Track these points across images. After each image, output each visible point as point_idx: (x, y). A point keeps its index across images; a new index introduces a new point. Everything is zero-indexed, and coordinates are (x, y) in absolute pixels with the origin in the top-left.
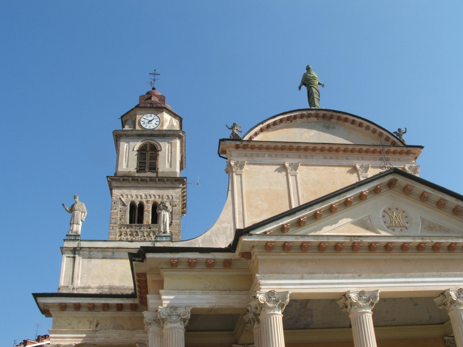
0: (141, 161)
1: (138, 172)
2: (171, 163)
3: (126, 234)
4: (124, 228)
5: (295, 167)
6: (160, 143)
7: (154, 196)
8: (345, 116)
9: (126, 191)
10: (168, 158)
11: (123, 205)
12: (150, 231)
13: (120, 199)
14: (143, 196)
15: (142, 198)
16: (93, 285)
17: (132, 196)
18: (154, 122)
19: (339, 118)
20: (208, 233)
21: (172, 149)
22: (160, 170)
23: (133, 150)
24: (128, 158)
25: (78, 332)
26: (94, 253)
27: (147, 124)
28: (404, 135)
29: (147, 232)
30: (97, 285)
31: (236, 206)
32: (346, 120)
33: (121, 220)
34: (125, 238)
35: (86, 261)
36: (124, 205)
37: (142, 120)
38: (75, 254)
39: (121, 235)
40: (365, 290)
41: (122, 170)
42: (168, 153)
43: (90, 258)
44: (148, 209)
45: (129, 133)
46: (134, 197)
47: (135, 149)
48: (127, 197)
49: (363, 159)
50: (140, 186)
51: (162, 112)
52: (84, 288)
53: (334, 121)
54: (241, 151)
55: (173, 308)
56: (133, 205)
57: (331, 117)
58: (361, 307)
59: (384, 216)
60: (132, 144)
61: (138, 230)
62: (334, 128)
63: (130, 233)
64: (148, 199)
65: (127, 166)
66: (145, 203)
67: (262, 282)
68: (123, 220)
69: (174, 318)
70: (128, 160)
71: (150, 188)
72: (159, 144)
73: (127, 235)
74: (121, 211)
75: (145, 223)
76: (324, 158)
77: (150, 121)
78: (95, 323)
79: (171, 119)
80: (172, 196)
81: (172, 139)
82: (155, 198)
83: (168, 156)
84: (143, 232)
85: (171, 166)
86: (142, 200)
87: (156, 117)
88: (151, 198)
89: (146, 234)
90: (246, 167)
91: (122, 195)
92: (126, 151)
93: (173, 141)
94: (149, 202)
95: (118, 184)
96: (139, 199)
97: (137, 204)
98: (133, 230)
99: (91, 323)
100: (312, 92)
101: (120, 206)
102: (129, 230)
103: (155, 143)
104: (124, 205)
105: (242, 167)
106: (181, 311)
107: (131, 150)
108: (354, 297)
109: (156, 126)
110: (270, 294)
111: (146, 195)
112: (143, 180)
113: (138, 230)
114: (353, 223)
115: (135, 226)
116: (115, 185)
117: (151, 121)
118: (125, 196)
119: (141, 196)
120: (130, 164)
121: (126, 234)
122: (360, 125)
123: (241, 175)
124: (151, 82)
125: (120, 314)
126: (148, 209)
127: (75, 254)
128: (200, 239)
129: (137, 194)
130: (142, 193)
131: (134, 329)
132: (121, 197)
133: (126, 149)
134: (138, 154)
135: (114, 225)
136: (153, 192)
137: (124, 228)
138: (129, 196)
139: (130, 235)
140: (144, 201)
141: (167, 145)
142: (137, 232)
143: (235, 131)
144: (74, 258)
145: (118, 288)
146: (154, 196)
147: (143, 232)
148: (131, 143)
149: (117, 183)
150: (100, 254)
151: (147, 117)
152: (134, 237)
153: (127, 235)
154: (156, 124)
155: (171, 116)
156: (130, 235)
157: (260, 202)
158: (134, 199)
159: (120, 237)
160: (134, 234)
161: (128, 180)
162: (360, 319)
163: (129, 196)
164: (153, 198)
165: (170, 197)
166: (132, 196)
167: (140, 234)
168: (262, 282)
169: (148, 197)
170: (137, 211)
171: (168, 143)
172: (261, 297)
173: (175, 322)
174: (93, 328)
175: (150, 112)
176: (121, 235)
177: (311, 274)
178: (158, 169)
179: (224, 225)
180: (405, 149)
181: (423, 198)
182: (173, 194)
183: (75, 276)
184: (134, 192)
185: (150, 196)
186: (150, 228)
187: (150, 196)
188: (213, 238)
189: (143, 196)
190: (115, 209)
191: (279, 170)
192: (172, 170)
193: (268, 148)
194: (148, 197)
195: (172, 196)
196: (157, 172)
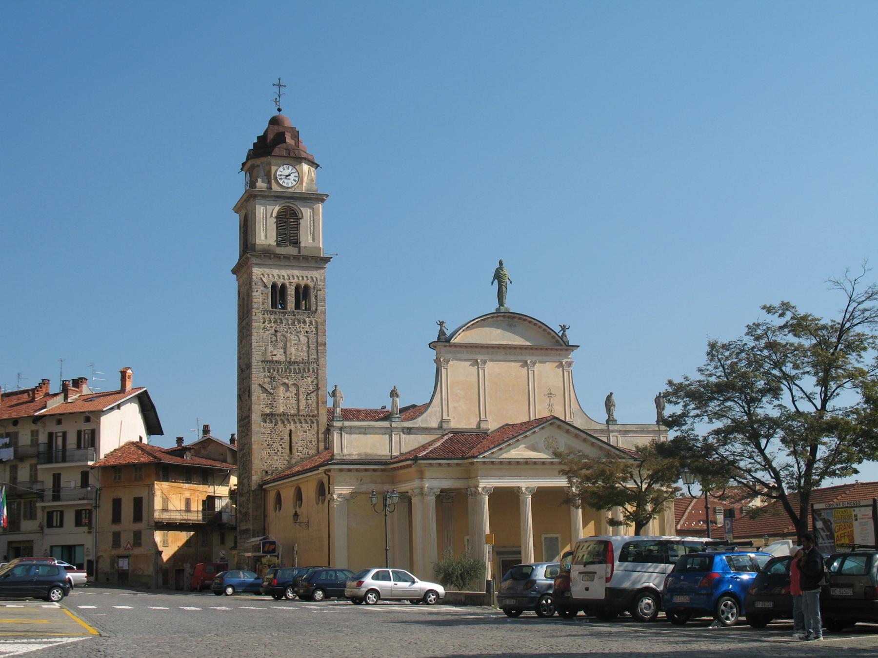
0: (281, 231)
1: (278, 245)
2: (314, 235)
3: (270, 321)
4: (268, 314)
5: (484, 362)
6: (301, 209)
7: (297, 276)
8: (525, 318)
9: (267, 271)
10: (310, 229)
11: (265, 287)
12: (294, 319)
13: (261, 278)
14: (286, 277)
15: (284, 279)
16: (355, 453)
17: (273, 276)
18: (292, 177)
19: (520, 319)
20: (425, 415)
21: (315, 217)
22: (302, 245)
23: (271, 216)
24: (266, 226)
25: (351, 486)
26: (353, 430)
27: (285, 180)
28: (567, 330)
29: (291, 319)
30: (357, 453)
31: (443, 395)
32: (525, 320)
33: (263, 304)
34: (269, 326)
35: (348, 435)
36: (265, 286)
37: (278, 173)
38: (341, 431)
39: (264, 323)
40: (530, 486)
41: (260, 242)
42: (310, 222)
43: (351, 433)
44: (291, 292)
45: (267, 194)
46: (276, 277)
47: (274, 215)
48: (269, 277)
49: (533, 354)
50: (282, 264)
51: (301, 163)
52: (349, 455)
53: (516, 320)
54: (448, 348)
55: (431, 489)
56: (274, 286)
57: (514, 317)
58: (526, 495)
59: (544, 442)
60: (270, 208)
61: (282, 318)
62: (515, 326)
63: (274, 320)
64: (291, 281)
65: (266, 237)
66: (288, 285)
67: (480, 481)
68: (265, 305)
69: (432, 494)
70: (266, 228)
71: (293, 267)
72: (300, 209)
73: (271, 322)
74: (262, 294)
75: (289, 309)
76: (506, 354)
77: (287, 176)
78: (360, 479)
79: (309, 168)
80: (316, 277)
81: (314, 204)
82: (299, 279)
83: (310, 225)
84: (287, 320)
85: (313, 240)
86: (285, 281)
87: (294, 170)
88: (294, 279)
89: (290, 322)
90: (451, 363)
91: (262, 274)
92: (263, 217)
93: (315, 207)
94: (293, 284)
95: (258, 261)
96: (281, 280)
97: (280, 285)
98: (277, 317)
99: (357, 479)
100: (502, 291)
101: (262, 288)
102: (272, 317)
103: (295, 207)
104: (265, 286)
105: (448, 362)
106: (436, 490)
107: (268, 216)
108: (524, 489)
109: (294, 183)
110: (483, 488)
111: (288, 276)
112: (287, 258)
113: (282, 318)
114: (525, 447)
115: (279, 312)
116: (255, 262)
117: (289, 175)
118: (266, 276)
119: (283, 276)
120: (268, 235)
121: (270, 321)
122: (535, 324)
123: (447, 369)
124: (276, 99)
125: (374, 473)
126: (291, 292)
127: (341, 431)
128: (420, 419)
129: (279, 273)
130: (284, 272)
131: (383, 483)
132: (262, 276)
133: (263, 213)
134: (276, 222)
135: (257, 311)
136: (296, 272)
137: (268, 314)
138: (271, 276)
139: (274, 322)
140: (287, 282)
141: (309, 211)
142: (281, 320)
143: (443, 328)
144: (341, 434)
145: (370, 455)
146: (297, 276)
147: (287, 320)
148: (268, 207)
149: (257, 259)
150: (357, 431)
151: (284, 169)
152: (278, 325)
153: (271, 322)
154: (295, 180)
155: (309, 165)
156: (274, 322)
157: (459, 391)
158: (276, 280)
159: (263, 325)
160: (279, 321)
161: (270, 257)
162: (525, 500)
163: (271, 276)
164: (296, 280)
165: (314, 278)
166: (273, 276)
167: (284, 322)
168: (480, 481)
169: (291, 278)
170: (278, 292)
171: (310, 208)
172: (480, 489)
173: (431, 496)
174: (359, 481)
175: (286, 162)
176: (264, 323)
177: (504, 477)
178: (300, 243)
179: (435, 409)
180: (566, 348)
181: (567, 431)
182: (317, 276)
183: (343, 447)
184: (276, 272)
185: (293, 276)
186: (295, 315)
187: (293, 276)
188: (428, 419)
189: (286, 277)
190: (257, 291)
191: (472, 365)
192: (315, 244)
193: (466, 347)
194: (291, 278)
195: (316, 277)
196: (299, 247)
